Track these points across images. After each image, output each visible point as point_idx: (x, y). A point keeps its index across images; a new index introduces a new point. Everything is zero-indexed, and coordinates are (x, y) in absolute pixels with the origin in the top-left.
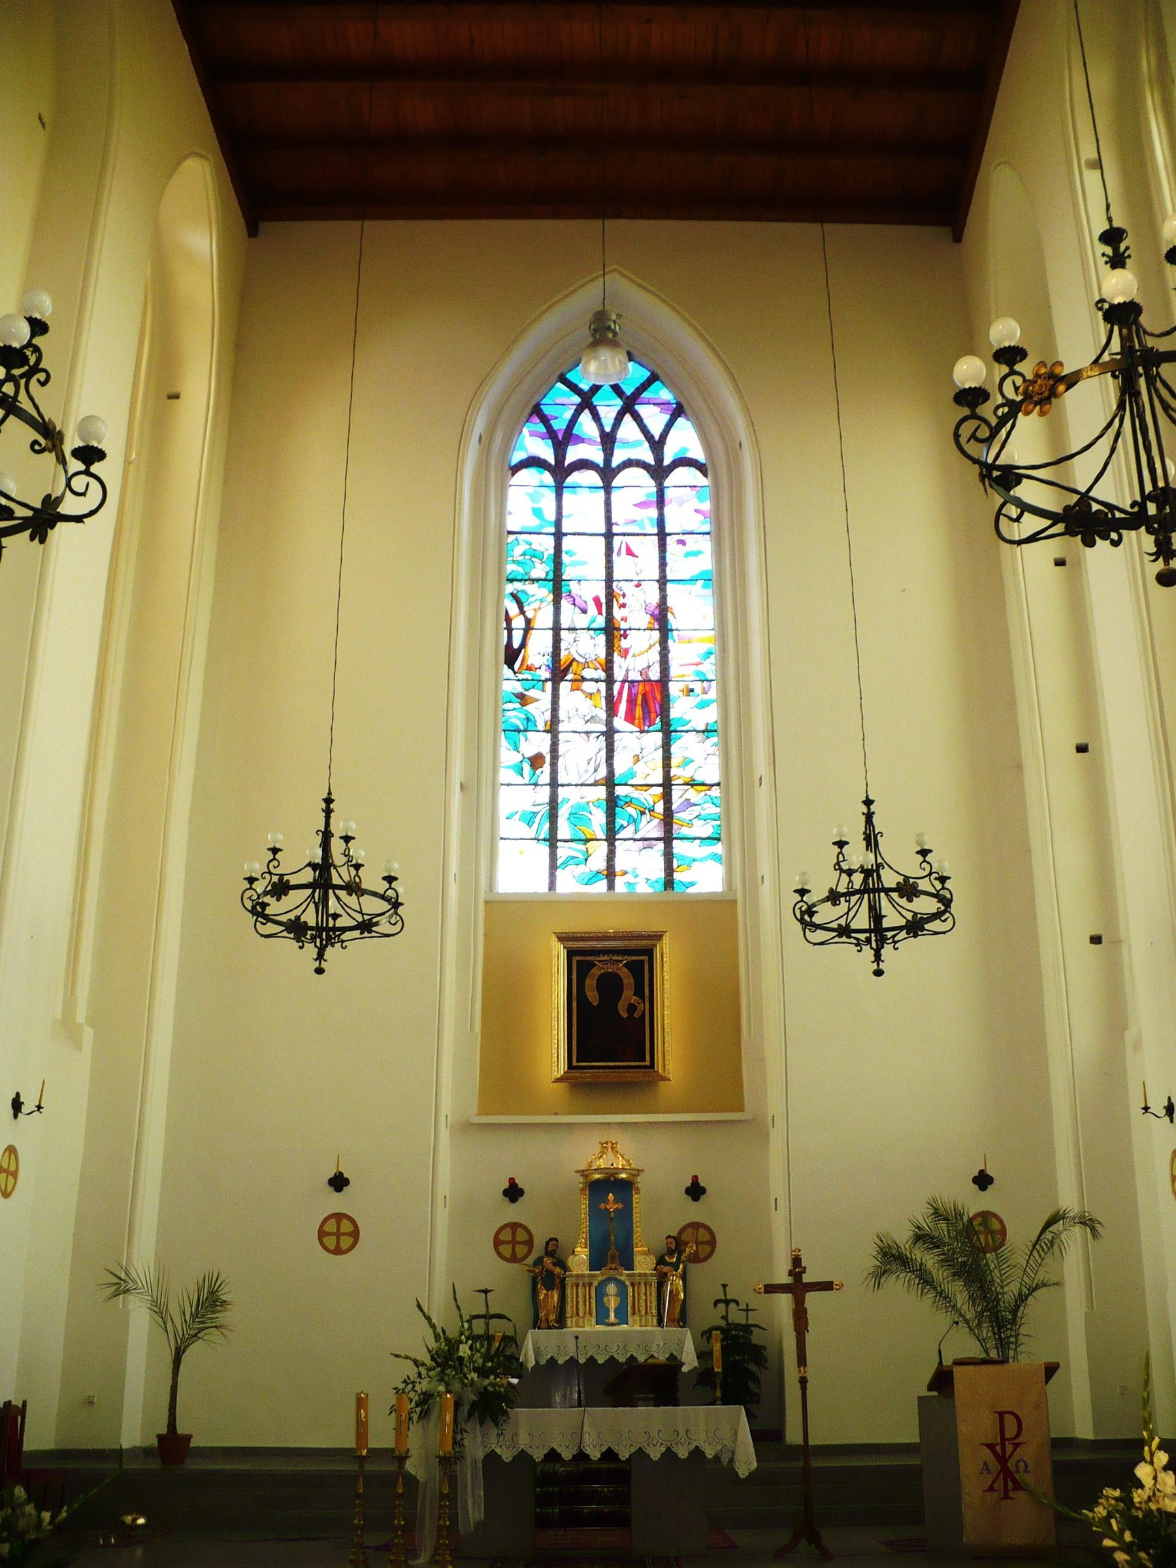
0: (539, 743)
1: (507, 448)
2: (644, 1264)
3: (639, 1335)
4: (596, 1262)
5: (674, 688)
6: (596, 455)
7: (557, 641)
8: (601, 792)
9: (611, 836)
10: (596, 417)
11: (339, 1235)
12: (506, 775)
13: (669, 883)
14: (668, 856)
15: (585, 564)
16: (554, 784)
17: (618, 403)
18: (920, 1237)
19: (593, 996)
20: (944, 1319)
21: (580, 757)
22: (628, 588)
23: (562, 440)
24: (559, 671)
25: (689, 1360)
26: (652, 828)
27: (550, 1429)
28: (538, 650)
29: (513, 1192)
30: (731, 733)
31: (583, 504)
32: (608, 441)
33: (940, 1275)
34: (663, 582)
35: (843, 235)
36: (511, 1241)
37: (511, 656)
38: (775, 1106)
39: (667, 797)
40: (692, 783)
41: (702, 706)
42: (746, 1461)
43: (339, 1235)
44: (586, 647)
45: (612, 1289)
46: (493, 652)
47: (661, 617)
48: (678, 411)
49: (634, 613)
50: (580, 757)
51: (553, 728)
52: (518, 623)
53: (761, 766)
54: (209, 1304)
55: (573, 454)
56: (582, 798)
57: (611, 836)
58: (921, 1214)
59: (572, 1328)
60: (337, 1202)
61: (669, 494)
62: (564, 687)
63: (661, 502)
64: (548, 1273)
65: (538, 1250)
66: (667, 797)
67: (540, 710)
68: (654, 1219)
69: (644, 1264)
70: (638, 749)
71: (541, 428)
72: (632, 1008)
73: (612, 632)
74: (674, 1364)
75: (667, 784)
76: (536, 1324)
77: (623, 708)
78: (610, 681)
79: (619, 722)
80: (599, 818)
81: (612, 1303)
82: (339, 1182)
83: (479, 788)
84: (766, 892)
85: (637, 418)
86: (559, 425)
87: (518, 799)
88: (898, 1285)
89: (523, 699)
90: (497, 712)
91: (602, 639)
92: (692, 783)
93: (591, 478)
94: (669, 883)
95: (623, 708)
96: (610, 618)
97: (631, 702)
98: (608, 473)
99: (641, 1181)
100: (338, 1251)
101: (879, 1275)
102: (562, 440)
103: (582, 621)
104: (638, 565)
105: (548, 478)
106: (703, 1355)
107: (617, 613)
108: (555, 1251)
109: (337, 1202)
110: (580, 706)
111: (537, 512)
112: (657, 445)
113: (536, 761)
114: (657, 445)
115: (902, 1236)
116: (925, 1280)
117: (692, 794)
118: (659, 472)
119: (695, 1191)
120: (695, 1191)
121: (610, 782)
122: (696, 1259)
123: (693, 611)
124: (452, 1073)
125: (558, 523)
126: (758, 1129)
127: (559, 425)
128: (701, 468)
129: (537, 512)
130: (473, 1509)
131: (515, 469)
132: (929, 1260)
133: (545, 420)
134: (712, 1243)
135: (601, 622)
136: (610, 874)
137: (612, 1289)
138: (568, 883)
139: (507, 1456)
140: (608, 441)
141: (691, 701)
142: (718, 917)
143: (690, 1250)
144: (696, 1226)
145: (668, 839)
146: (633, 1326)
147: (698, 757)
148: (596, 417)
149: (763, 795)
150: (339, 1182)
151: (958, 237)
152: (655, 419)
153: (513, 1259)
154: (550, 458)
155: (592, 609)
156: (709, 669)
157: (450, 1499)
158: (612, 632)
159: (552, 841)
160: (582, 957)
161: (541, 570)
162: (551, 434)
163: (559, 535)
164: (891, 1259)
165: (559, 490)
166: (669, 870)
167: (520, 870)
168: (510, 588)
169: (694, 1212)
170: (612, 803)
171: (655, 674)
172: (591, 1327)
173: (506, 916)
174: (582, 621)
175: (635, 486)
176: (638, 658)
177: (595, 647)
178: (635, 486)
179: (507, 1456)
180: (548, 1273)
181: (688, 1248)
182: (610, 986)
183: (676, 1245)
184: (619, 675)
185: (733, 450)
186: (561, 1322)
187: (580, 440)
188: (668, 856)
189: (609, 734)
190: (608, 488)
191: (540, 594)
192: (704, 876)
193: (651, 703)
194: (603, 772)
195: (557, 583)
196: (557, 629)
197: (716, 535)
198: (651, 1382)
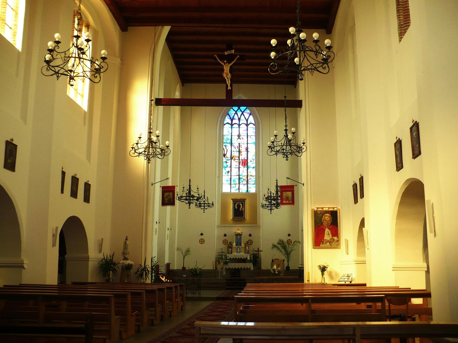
0: (229, 169)
1: (223, 122)
2: (243, 245)
3: (242, 255)
4: (236, 245)
5: (249, 161)
6: (237, 122)
7: (231, 153)
8: (238, 177)
9: (239, 184)
10: (237, 115)
11: (202, 241)
12: (224, 174)
13: (247, 191)
14: (247, 187)
15: (236, 142)
16: (231, 176)
17: (241, 113)
18: (278, 243)
19: (236, 208)
20: (281, 254)
21: (235, 171)
22: (242, 144)
23: (232, 119)
24: (232, 158)
25: (249, 258)
26: (245, 182)
27: (233, 266)
28: (228, 155)
29: (225, 235)
30: (257, 168)
31: (235, 131)
32: (239, 119)
33: (281, 248)
34: (247, 143)
35: (277, 86)
36: (225, 242)
37: (224, 155)
38: (261, 224)
39: (247, 178)
40: (251, 176)
41: (253, 163)
42: (252, 268)
43: (202, 241)
44: (236, 154)
45: (238, 249)
46: (222, 155)
47: (247, 149)
48: (250, 115)
49: (243, 149)
50: (235, 171)
51: (231, 167)
52: (226, 150)
53: (261, 175)
54: (188, 251)
55: (234, 122)
56: (235, 178)
57: (239, 184)
58: (278, 240)
59: (233, 254)
60: (202, 237)
61: (248, 129)
62: (232, 160)
63: (247, 130)
64: (230, 246)
65: (229, 242)
66: (247, 178)
67: (229, 164)
68: (245, 239)
69: (243, 245)
70: (243, 170)
71: (229, 117)
72: (242, 209)
73: (239, 152)
74: (247, 258)
75: (247, 176)
76: (228, 253)
77: (241, 164)
78: (239, 159)
79: (241, 166)
80: (237, 182)
81: (239, 250)
82: (202, 234)
83: (220, 177)
84: (261, 193)
85: (244, 115)
86: (232, 117)
87: (226, 178)
88: (275, 249)
89: (226, 162)
90: (223, 164)
91: (238, 153)
92: (251, 176)
93: (237, 126)
94: (247, 191)
95: (241, 164)
96: (239, 149)
97: (242, 163)
98: (239, 125)
99: (243, 234)
100: (202, 244)
101: (273, 248)
102: (232, 119)
103: (235, 150)
104: (243, 141)
105: (230, 126)
106: (250, 258)
107: (240, 148)
108: (231, 244)
109: (202, 237)
110: (235, 163)
111: (228, 132)
112: (247, 120)
113: (228, 172)
114: (247, 120)
115: (276, 243)
116: (278, 249)
117: (251, 177)
118: (247, 125)
119: (250, 235)
120: (250, 235)
121: (239, 175)
122: (250, 244)
123: (252, 149)
124: (217, 219)
125: (232, 134)
126: (259, 227)
127: (232, 117)
128: (254, 125)
129: (228, 132)
130: (224, 273)
131: (225, 125)
132: (279, 246)
133: (229, 115)
134: (252, 242)
135: (238, 150)
136: (239, 189)
137: (238, 249)
138: (233, 191)
139: (228, 268)
140: (239, 119)
141: (251, 163)
142: (254, 196)
143: (249, 243)
144: (250, 240)
145: (247, 184)
146: (241, 254)
147: (252, 172)
148: (237, 115)
149: (261, 179)
150: (202, 234)
151: (295, 87)
152: (247, 115)
153: (225, 244)
154: (230, 122)
155: (237, 148)
156: (254, 158)
157: (222, 272)
158: (239, 152)
159: (231, 184)
160: (235, 201)
161: (229, 141)
162: (230, 118)
163: (232, 136)
164: (274, 246)
165: (232, 128)
166: (247, 189)
167: (226, 189)
168: (224, 144)
169: (250, 238)
170: (239, 178)
171: (246, 159)
172: (236, 254)
173: (225, 196)
174: (235, 150)
175: (243, 127)
176: (243, 156)
177: (237, 154)
178: (243, 127)
179: (228, 268)
180: (230, 246)
181: (249, 243)
182: (239, 206)
183: (248, 243)
184: (240, 159)
185: (258, 123)
186: (232, 253)
187: (235, 119)
188: (247, 187)
189: (239, 168)
190: (239, 128)
191: (229, 145)
192: (252, 190)
193: (245, 163)
194: (238, 174)
195: (231, 144)
196: (231, 151)
197: (256, 136)
198: (243, 260)
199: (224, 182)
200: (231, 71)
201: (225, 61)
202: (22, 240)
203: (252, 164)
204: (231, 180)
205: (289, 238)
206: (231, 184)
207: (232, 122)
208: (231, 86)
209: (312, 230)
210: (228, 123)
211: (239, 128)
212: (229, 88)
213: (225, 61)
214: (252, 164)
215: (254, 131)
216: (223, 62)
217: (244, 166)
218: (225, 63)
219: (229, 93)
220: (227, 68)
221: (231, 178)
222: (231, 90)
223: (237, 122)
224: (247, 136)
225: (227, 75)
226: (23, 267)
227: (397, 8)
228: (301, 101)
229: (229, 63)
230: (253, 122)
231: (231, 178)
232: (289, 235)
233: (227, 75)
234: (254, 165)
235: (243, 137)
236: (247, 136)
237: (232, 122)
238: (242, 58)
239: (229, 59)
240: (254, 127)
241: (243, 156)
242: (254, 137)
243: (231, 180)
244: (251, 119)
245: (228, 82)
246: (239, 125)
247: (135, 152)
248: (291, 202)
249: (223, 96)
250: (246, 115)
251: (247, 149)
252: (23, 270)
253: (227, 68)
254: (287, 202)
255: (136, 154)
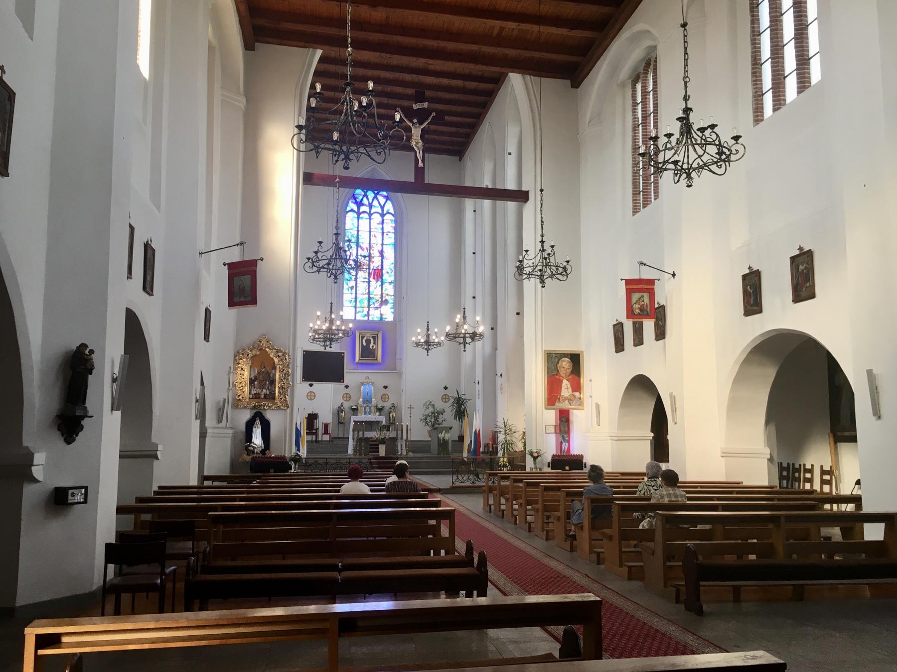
0: (352, 283)
5: (384, 271)
8: (367, 296)
9: (369, 306)
12: (345, 291)
21: (362, 287)
30: (397, 283)
31: (364, 223)
34: (382, 244)
47: (381, 253)
49: (375, 253)
50: (362, 287)
51: (356, 280)
57: (369, 306)
73: (370, 256)
78: (369, 269)
79: (371, 279)
86: (358, 200)
93: (366, 216)
98: (370, 215)
105: (355, 215)
112: (382, 208)
113: (352, 288)
114: (382, 208)
118: (383, 215)
121: (369, 293)
123: (390, 253)
126: (400, 374)
135: (367, 254)
136: (368, 315)
138: (359, 317)
140: (370, 206)
147: (389, 289)
156: (392, 267)
159: (355, 307)
163: (358, 231)
170: (369, 298)
175: (377, 218)
176: (376, 263)
178: (377, 218)
182: (368, 341)
187: (363, 205)
189: (369, 282)
190: (370, 219)
191: (354, 245)
193: (378, 274)
197: (395, 233)
199: (345, 304)
200: (422, 137)
201: (415, 121)
202: (154, 411)
203: (389, 277)
204: (356, 301)
205: (446, 392)
206: (355, 307)
207: (383, 210)
208: (423, 161)
209: (17, 285)
210: (352, 210)
211: (370, 219)
212: (421, 164)
213: (415, 121)
214: (389, 277)
215: (394, 225)
216: (411, 121)
217: (377, 280)
218: (413, 124)
219: (420, 172)
220: (416, 132)
221: (356, 298)
222: (423, 168)
223: (366, 209)
224: (383, 233)
225: (416, 140)
226: (157, 458)
227: (753, 69)
228: (527, 193)
229: (421, 124)
230: (392, 211)
231: (356, 298)
232: (446, 388)
233: (416, 140)
234: (392, 279)
235: (377, 234)
236: (383, 233)
237: (383, 210)
238: (440, 116)
239: (421, 116)
240: (393, 218)
241: (376, 263)
242: (393, 236)
243: (356, 301)
244: (389, 206)
245: (420, 156)
246: (370, 215)
247: (313, 265)
248: (249, 298)
249: (411, 178)
250: (382, 202)
251: (381, 253)
252: (155, 462)
253: (416, 132)
254: (242, 299)
255: (315, 269)
